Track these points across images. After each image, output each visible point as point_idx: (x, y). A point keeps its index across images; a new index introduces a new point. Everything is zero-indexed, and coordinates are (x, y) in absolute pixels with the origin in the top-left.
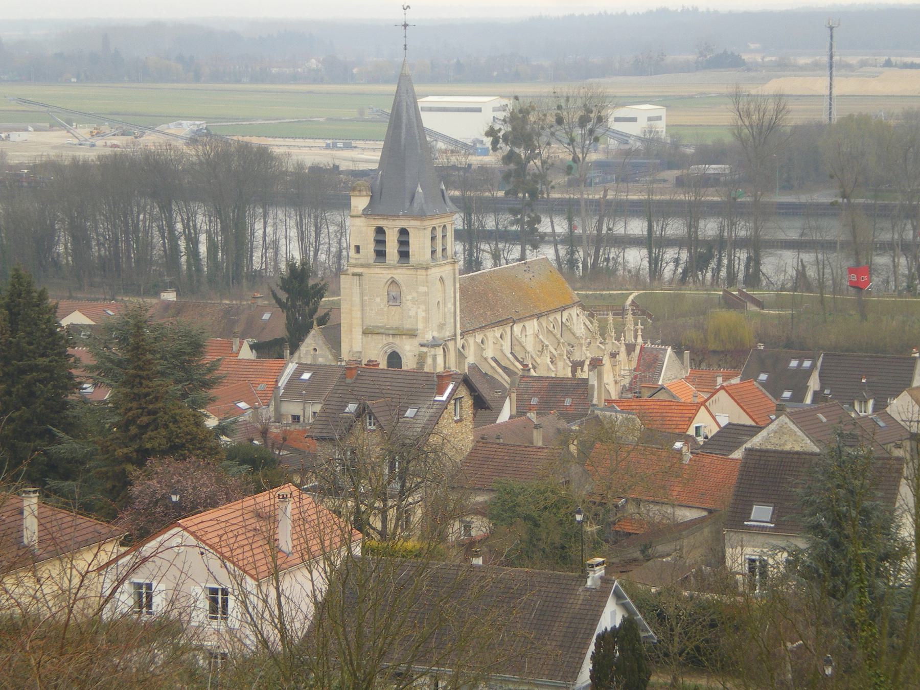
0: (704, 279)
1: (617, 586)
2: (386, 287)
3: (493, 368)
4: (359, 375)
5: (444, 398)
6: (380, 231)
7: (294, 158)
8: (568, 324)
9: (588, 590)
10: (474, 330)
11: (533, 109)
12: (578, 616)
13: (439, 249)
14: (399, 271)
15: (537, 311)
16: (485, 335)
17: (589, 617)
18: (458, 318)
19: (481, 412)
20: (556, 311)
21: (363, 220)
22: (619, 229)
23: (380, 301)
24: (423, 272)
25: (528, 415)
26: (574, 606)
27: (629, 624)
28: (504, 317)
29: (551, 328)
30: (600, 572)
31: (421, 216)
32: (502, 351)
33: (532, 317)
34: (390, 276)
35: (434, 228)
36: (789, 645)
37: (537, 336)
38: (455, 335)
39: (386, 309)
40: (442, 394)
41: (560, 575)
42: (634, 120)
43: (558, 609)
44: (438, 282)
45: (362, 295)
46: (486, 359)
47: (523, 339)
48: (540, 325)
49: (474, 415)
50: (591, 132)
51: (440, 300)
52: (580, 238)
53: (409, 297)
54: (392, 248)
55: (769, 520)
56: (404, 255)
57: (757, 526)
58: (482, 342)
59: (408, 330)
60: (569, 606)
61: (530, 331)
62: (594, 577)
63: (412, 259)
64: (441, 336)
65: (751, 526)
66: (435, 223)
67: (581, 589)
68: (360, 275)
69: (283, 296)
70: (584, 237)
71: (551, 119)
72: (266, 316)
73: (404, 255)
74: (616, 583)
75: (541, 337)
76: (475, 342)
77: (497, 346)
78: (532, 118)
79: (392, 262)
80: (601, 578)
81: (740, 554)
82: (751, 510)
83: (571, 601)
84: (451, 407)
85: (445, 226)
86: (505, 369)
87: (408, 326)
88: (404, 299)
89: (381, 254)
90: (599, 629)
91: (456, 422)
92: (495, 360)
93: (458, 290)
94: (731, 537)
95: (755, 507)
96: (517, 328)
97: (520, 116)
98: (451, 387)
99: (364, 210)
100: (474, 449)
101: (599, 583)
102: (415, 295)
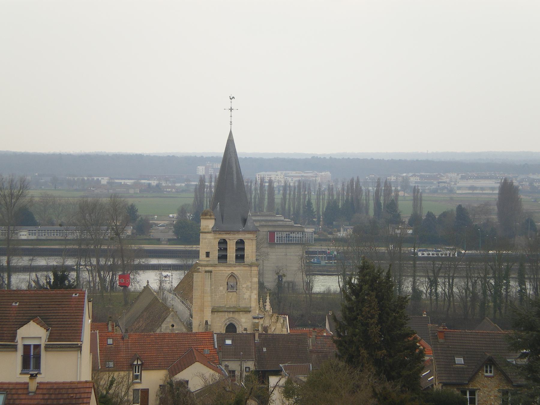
6: (223, 243)
14: (237, 268)
21: (212, 234)
34: (231, 272)
53: (244, 286)
54: (231, 253)
56: (240, 257)
68: (211, 272)
73: (240, 257)
89: (223, 257)
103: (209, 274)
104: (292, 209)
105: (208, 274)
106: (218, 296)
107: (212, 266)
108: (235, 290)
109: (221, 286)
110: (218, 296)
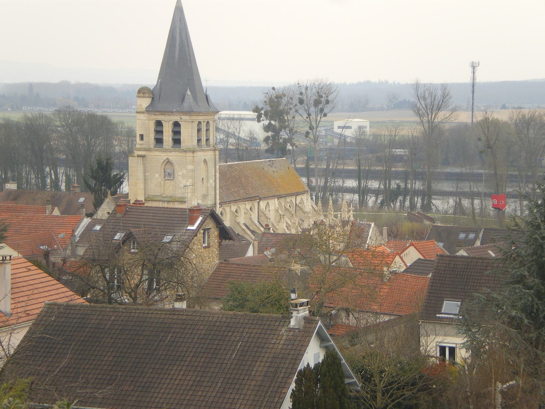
0: (394, 207)
1: (320, 327)
2: (163, 166)
3: (243, 230)
4: (127, 211)
5: (194, 227)
6: (159, 124)
7: (126, 125)
8: (300, 205)
9: (290, 330)
10: (230, 202)
11: (284, 95)
12: (280, 356)
13: (204, 139)
14: (173, 154)
15: (277, 194)
16: (238, 207)
17: (290, 357)
18: (218, 192)
19: (226, 242)
20: (291, 195)
21: (146, 115)
22: (339, 183)
23: (157, 177)
24: (190, 154)
25: (265, 253)
26: (276, 346)
27: (331, 361)
28: (253, 195)
29: (288, 207)
30: (304, 312)
31: (190, 113)
32: (251, 219)
33: (273, 197)
34: (166, 158)
35: (200, 123)
36: (499, 385)
37: (277, 211)
38: (215, 204)
39: (162, 182)
40: (193, 224)
41: (263, 317)
42: (349, 127)
43: (260, 350)
44: (202, 163)
45: (145, 172)
46: (238, 223)
47: (267, 212)
48: (280, 203)
49: (220, 244)
50: (322, 110)
51: (204, 177)
52: (313, 170)
53: (180, 173)
54: (168, 136)
55: (457, 312)
56: (177, 142)
57: (447, 318)
58: (236, 211)
59: (179, 198)
60: (271, 346)
61: (272, 207)
62: (298, 317)
63: (183, 144)
64: (205, 203)
65: (442, 318)
66: (201, 118)
67: (284, 329)
68: (143, 156)
69: (93, 183)
70: (317, 187)
71: (296, 101)
72: (82, 200)
73: (177, 142)
74: (320, 323)
75: (280, 212)
76: (231, 211)
77: (248, 216)
78: (284, 100)
79: (167, 147)
80: (305, 318)
81: (432, 342)
82: (442, 304)
83: (273, 342)
84: (200, 236)
85: (208, 122)
86: (253, 232)
87: (179, 195)
88: (176, 174)
89: (159, 141)
90: (301, 366)
91: (204, 248)
92: (246, 226)
93: (218, 171)
94: (425, 327)
95: (445, 302)
96: (263, 204)
97: (276, 100)
98: (200, 219)
99: (146, 108)
100: (218, 268)
101: (303, 323)
102: (185, 171)
103: (142, 158)
104: (178, 37)
105: (140, 159)
106: (153, 184)
107: (145, 150)
108: (172, 178)
109: (156, 173)
110: (153, 184)
